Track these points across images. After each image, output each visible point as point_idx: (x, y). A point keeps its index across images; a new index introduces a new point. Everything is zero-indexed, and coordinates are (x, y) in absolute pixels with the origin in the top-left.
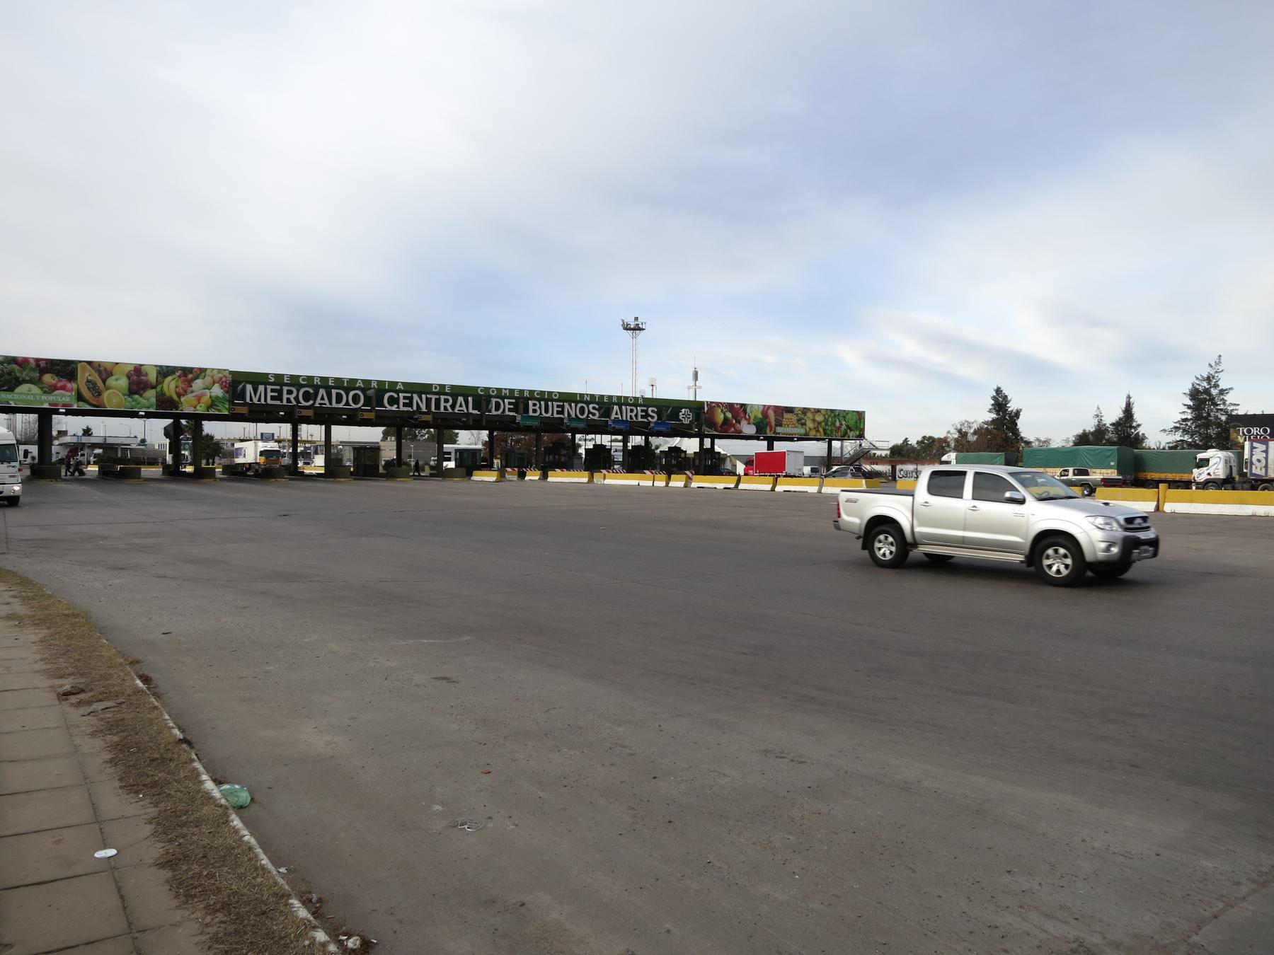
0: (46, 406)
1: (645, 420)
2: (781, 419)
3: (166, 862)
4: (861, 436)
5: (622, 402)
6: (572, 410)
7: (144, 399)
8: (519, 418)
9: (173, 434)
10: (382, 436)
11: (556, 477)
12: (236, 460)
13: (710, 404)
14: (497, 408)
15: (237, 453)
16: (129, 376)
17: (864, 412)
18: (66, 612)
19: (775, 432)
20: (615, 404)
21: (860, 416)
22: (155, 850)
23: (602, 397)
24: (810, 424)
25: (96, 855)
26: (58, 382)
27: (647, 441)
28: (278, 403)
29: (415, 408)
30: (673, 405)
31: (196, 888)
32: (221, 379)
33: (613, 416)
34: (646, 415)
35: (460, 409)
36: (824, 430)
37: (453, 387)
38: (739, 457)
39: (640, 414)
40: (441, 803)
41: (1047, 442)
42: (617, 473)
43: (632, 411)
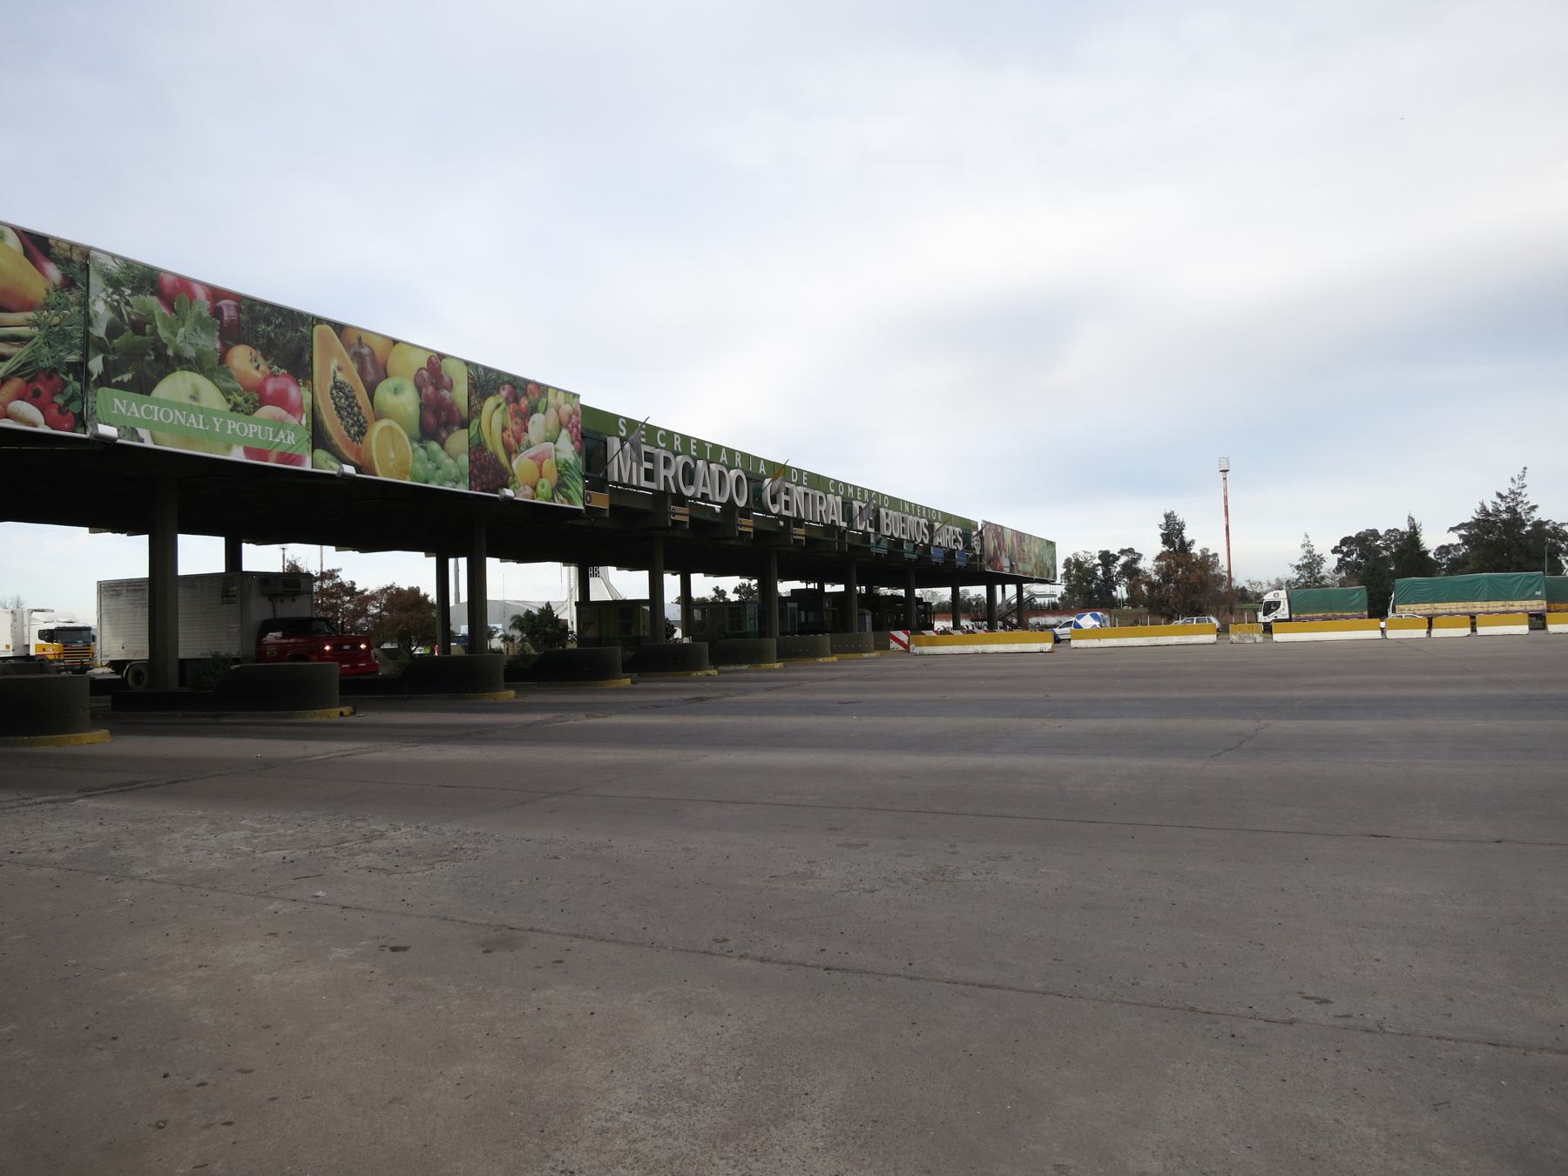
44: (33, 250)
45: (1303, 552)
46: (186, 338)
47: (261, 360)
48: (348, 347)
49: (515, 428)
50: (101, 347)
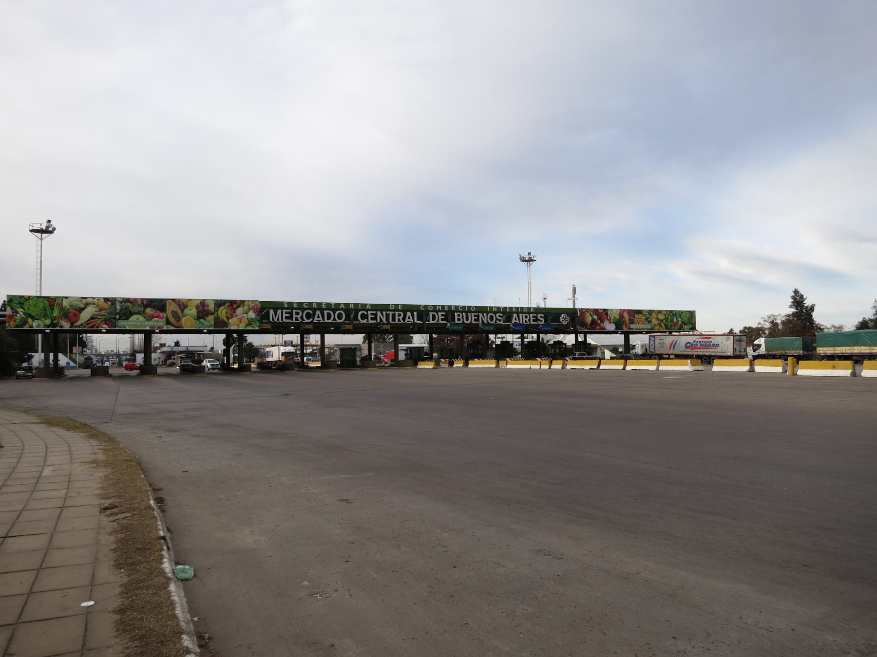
0: (148, 328)
1: (536, 323)
2: (633, 318)
3: (119, 610)
4: (693, 328)
5: (519, 311)
6: (484, 318)
7: (207, 322)
8: (448, 325)
9: (227, 343)
10: (363, 340)
11: (474, 364)
12: (267, 359)
13: (581, 310)
14: (434, 318)
15: (267, 354)
16: (197, 308)
17: (695, 311)
18: (127, 458)
19: (629, 328)
20: (514, 313)
21: (692, 314)
22: (116, 603)
23: (505, 308)
24: (655, 321)
25: (82, 605)
26: (154, 313)
27: (538, 337)
28: (290, 321)
29: (379, 321)
30: (555, 312)
31: (130, 626)
32: (254, 307)
33: (513, 321)
34: (537, 320)
35: (409, 320)
36: (665, 325)
37: (403, 305)
38: (607, 347)
39: (532, 319)
40: (309, 581)
41: (841, 327)
42: (518, 360)
43: (526, 317)
44: (106, 301)
46: (135, 309)
47: (153, 310)
48: (176, 303)
49: (231, 312)
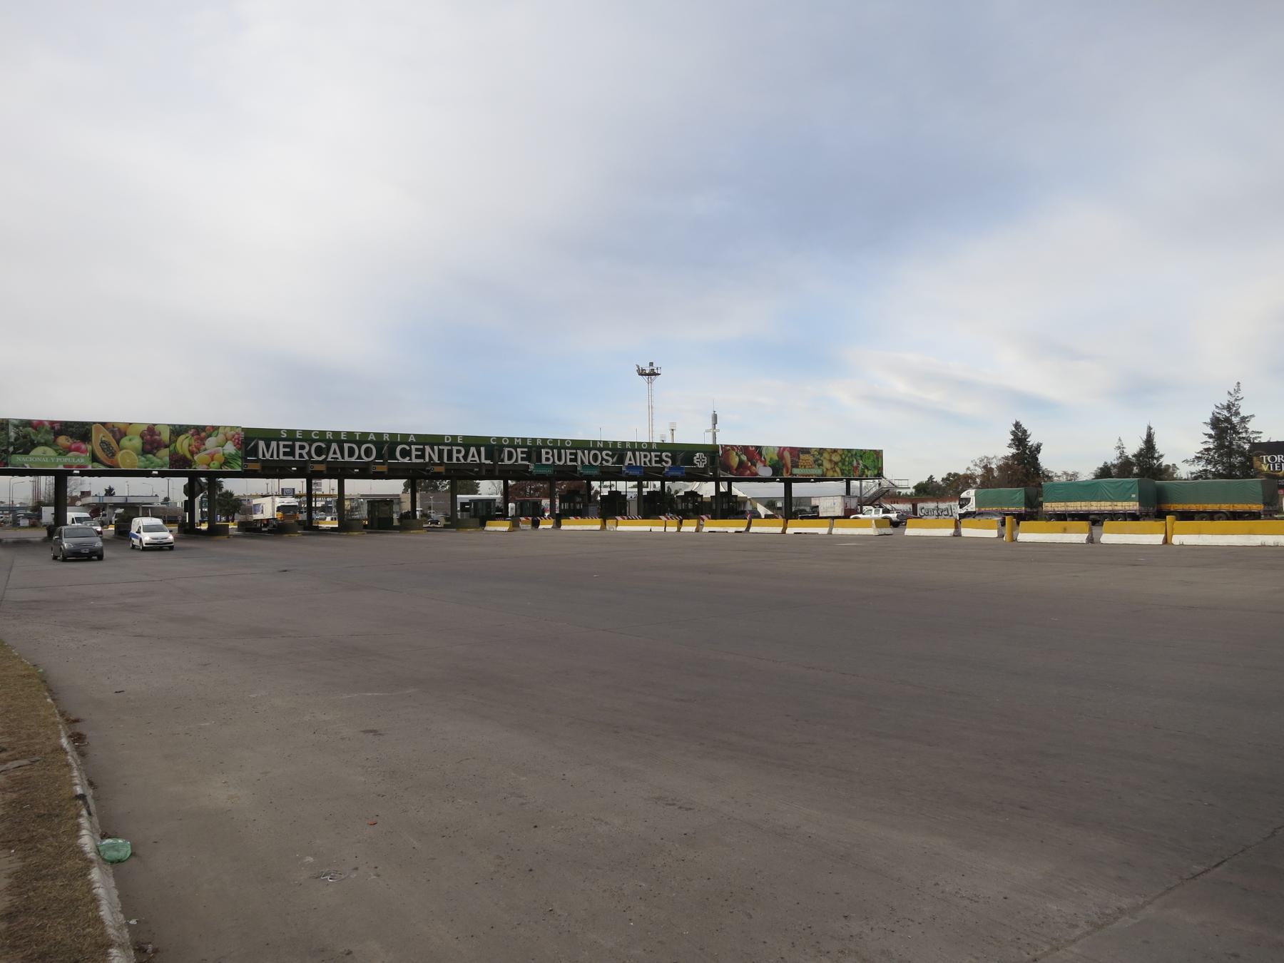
45: (1117, 453)
46: (40, 438)
47: (69, 439)
48: (107, 429)
50: (12, 444)
